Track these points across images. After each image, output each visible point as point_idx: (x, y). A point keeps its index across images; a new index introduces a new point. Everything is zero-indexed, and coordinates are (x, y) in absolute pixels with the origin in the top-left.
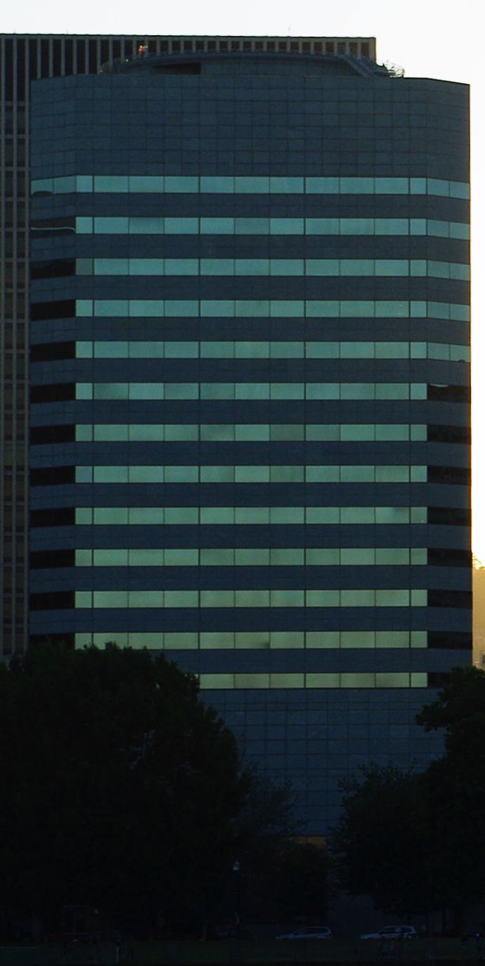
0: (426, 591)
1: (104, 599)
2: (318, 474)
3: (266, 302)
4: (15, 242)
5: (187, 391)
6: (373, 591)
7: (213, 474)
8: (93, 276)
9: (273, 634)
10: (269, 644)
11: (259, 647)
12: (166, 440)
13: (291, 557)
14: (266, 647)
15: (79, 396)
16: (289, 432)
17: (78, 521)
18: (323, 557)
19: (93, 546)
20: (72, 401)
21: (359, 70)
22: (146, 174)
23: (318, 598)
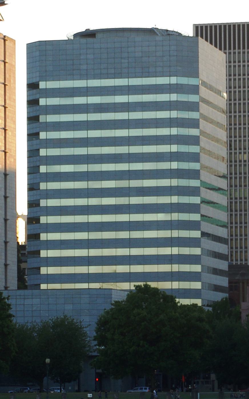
0: (200, 271)
1: (52, 270)
2: (135, 200)
3: (114, 130)
4: (243, 230)
5: (83, 168)
6: (156, 248)
7: (93, 201)
8: (178, 162)
9: (117, 266)
10: (116, 271)
11: (113, 272)
12: (75, 188)
13: (124, 235)
14: (115, 272)
15: (41, 171)
16: (123, 184)
17: (41, 239)
18: (137, 235)
19: (47, 249)
20: (38, 291)
21: (158, 33)
22: (66, 80)
23: (135, 252)
